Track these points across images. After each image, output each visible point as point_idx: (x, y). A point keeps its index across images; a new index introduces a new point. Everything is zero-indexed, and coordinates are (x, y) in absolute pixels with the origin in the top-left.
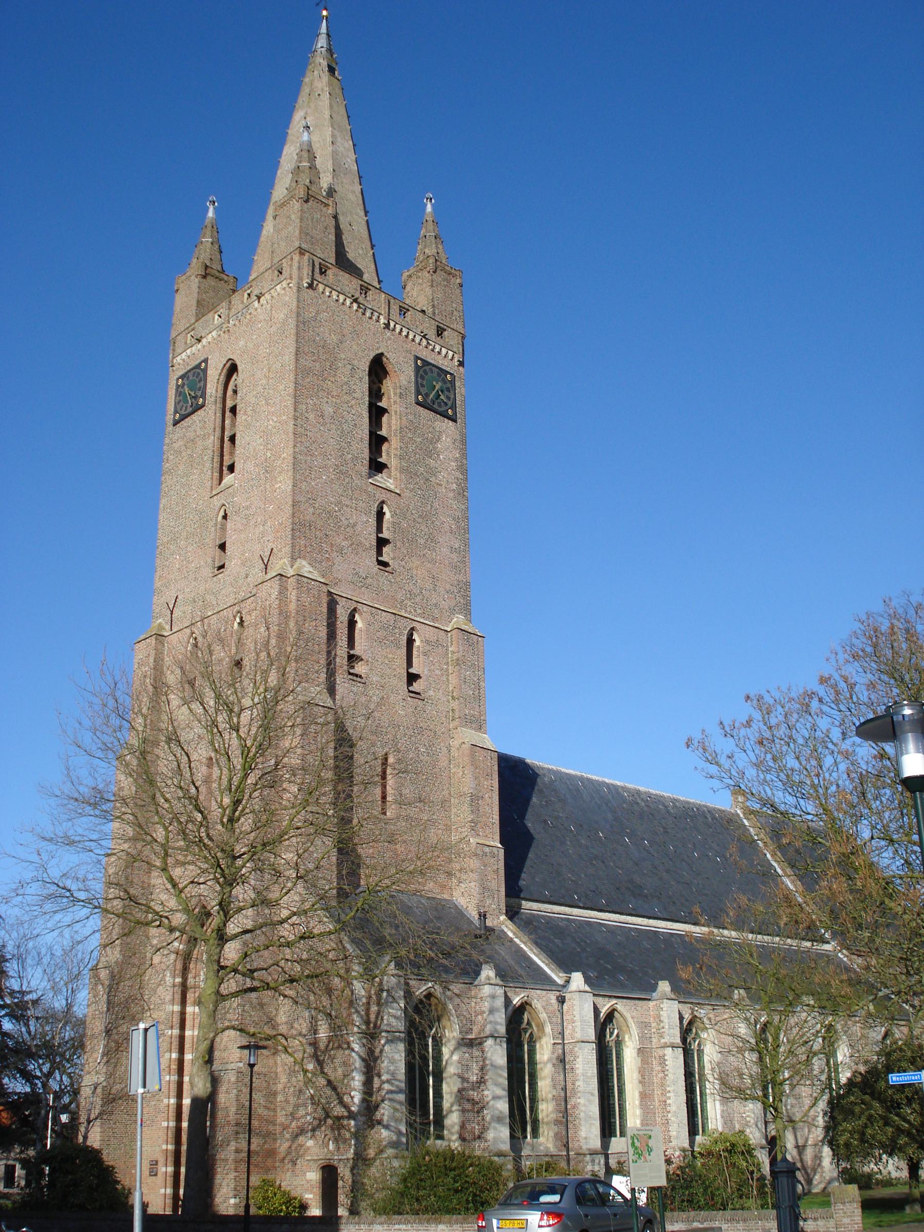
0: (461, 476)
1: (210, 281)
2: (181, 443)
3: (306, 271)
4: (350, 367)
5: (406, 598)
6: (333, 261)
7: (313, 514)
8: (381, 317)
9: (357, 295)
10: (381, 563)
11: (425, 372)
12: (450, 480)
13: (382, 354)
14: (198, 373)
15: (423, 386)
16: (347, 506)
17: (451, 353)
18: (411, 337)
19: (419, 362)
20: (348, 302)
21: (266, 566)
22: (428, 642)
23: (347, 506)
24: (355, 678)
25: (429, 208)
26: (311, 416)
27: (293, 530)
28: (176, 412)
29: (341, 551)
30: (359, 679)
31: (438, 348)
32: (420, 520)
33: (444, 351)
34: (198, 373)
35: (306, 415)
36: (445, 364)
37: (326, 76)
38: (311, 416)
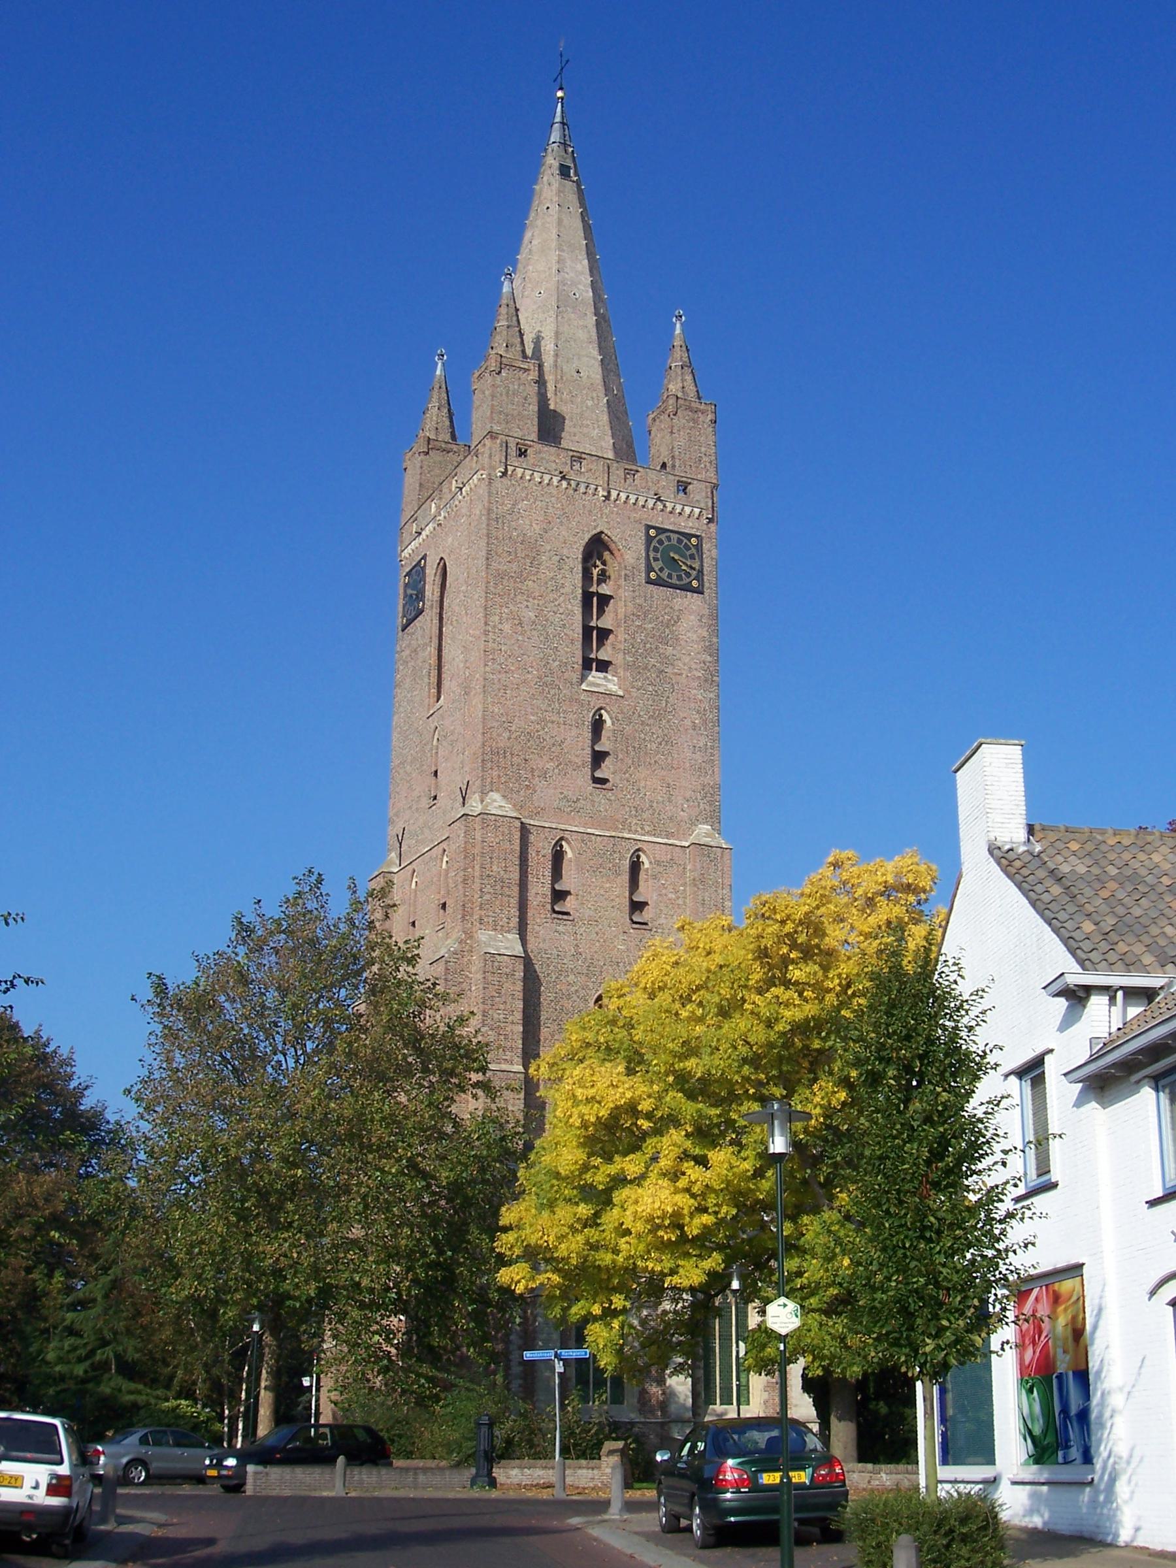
0: (709, 659)
1: (435, 456)
2: (407, 652)
3: (499, 457)
4: (558, 558)
5: (630, 816)
6: (534, 437)
7: (509, 738)
8: (600, 489)
9: (566, 469)
10: (597, 780)
11: (660, 542)
12: (694, 666)
13: (602, 532)
14: (418, 571)
15: (656, 559)
16: (553, 722)
17: (697, 511)
18: (641, 503)
19: (652, 532)
20: (555, 480)
21: (464, 799)
22: (658, 863)
23: (553, 722)
24: (560, 916)
25: (678, 330)
26: (507, 627)
27: (483, 760)
28: (404, 616)
29: (544, 775)
30: (565, 917)
31: (678, 509)
32: (651, 721)
33: (688, 510)
34: (418, 571)
35: (500, 626)
36: (688, 526)
37: (556, 180)
38: (507, 627)
